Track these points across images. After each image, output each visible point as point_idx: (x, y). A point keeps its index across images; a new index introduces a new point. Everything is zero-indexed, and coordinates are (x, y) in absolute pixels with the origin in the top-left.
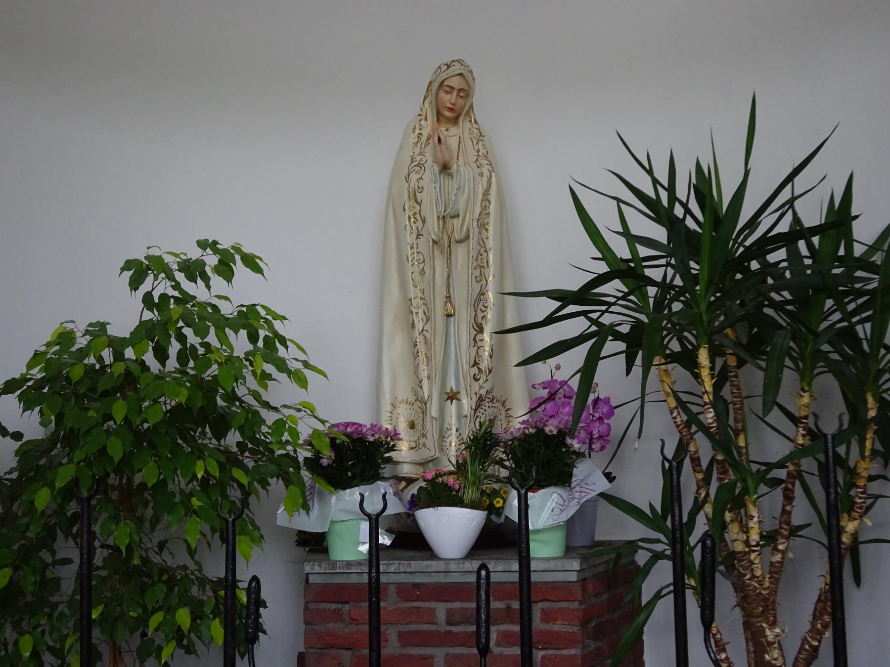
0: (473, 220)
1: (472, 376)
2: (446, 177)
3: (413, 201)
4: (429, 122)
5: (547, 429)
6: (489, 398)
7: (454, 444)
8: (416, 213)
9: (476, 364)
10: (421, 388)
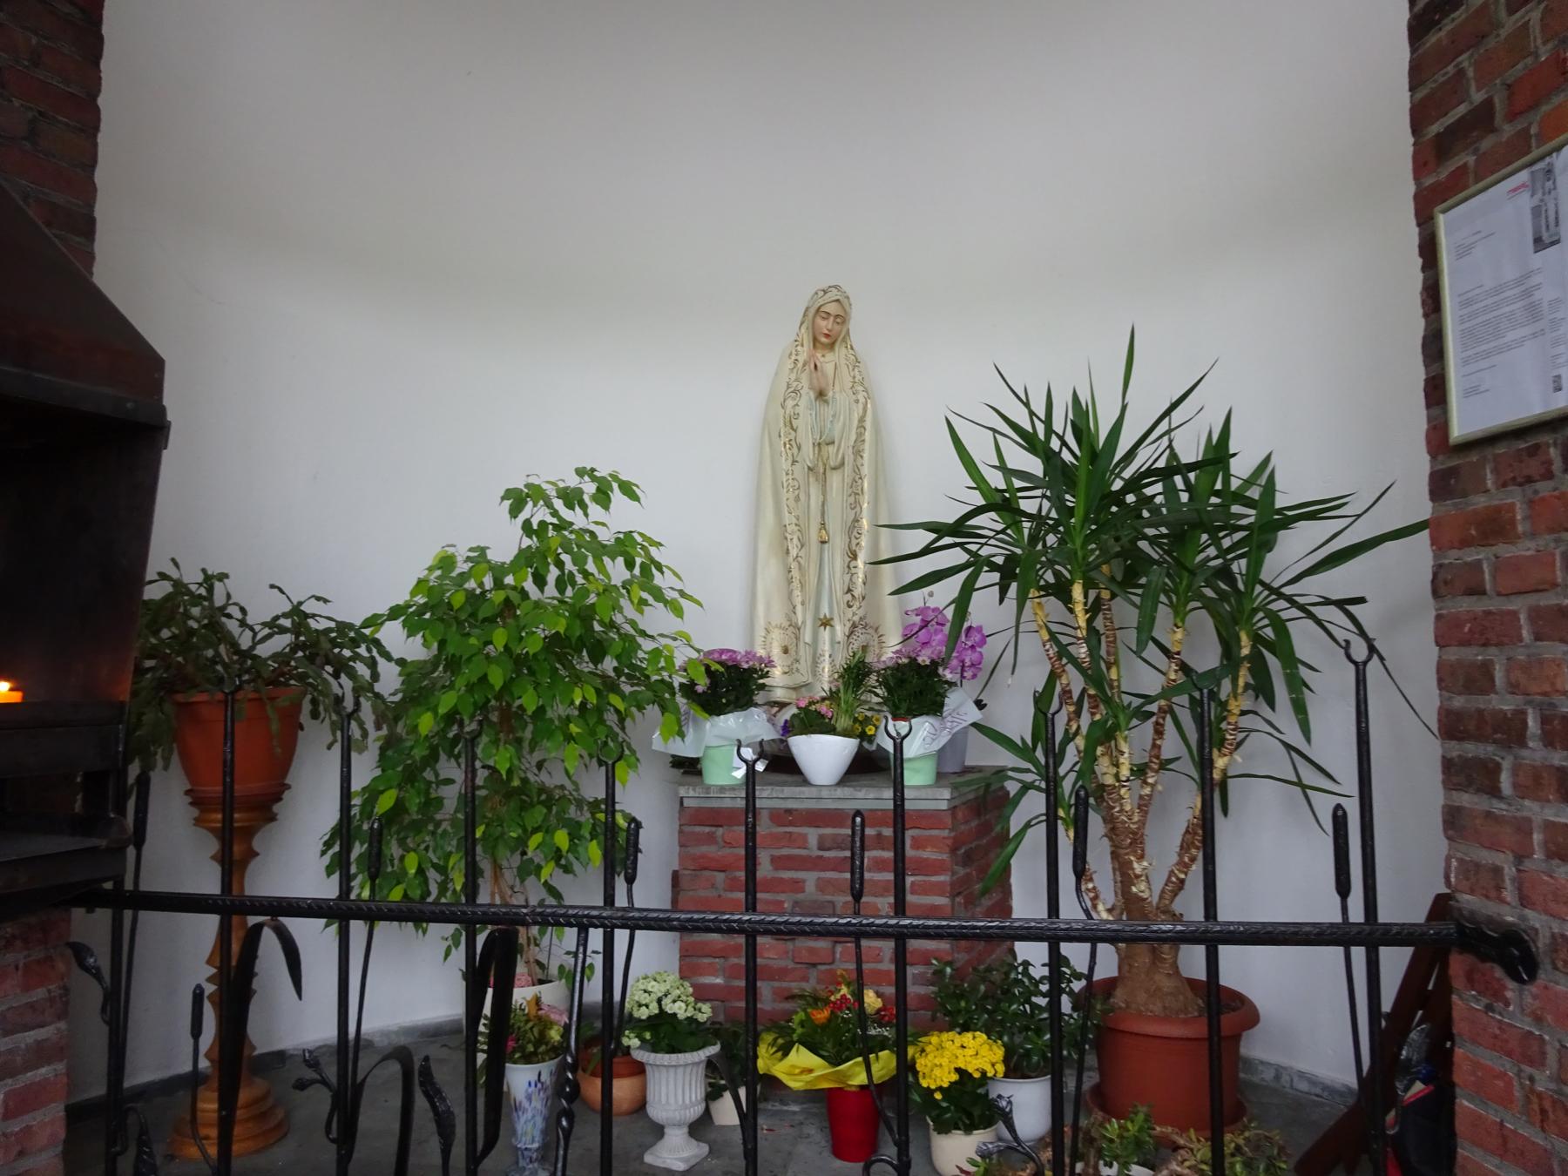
3: (788, 428)
4: (805, 348)
7: (826, 670)
9: (849, 590)
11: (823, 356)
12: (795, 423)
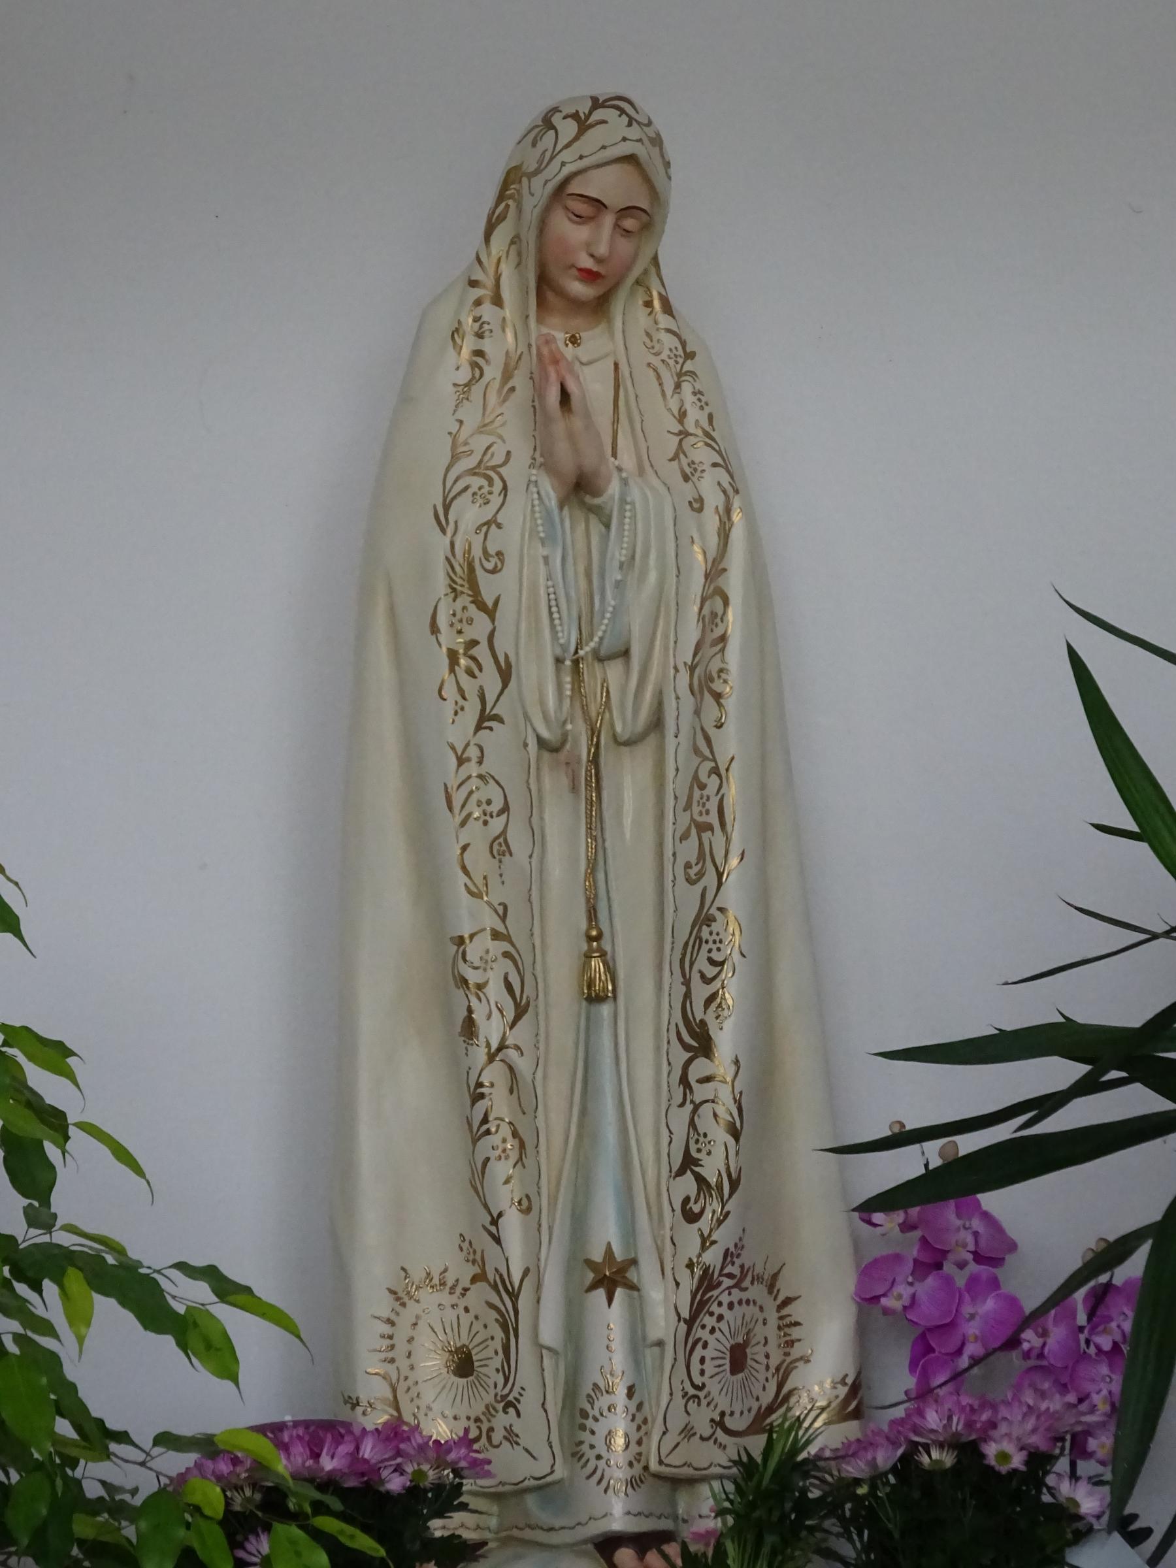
0: (676, 670)
1: (677, 1206)
2: (579, 514)
3: (464, 600)
4: (509, 311)
5: (991, 1450)
6: (730, 1276)
7: (620, 1441)
8: (474, 643)
9: (689, 1162)
10: (497, 1240)
11: (574, 340)
12: (489, 588)
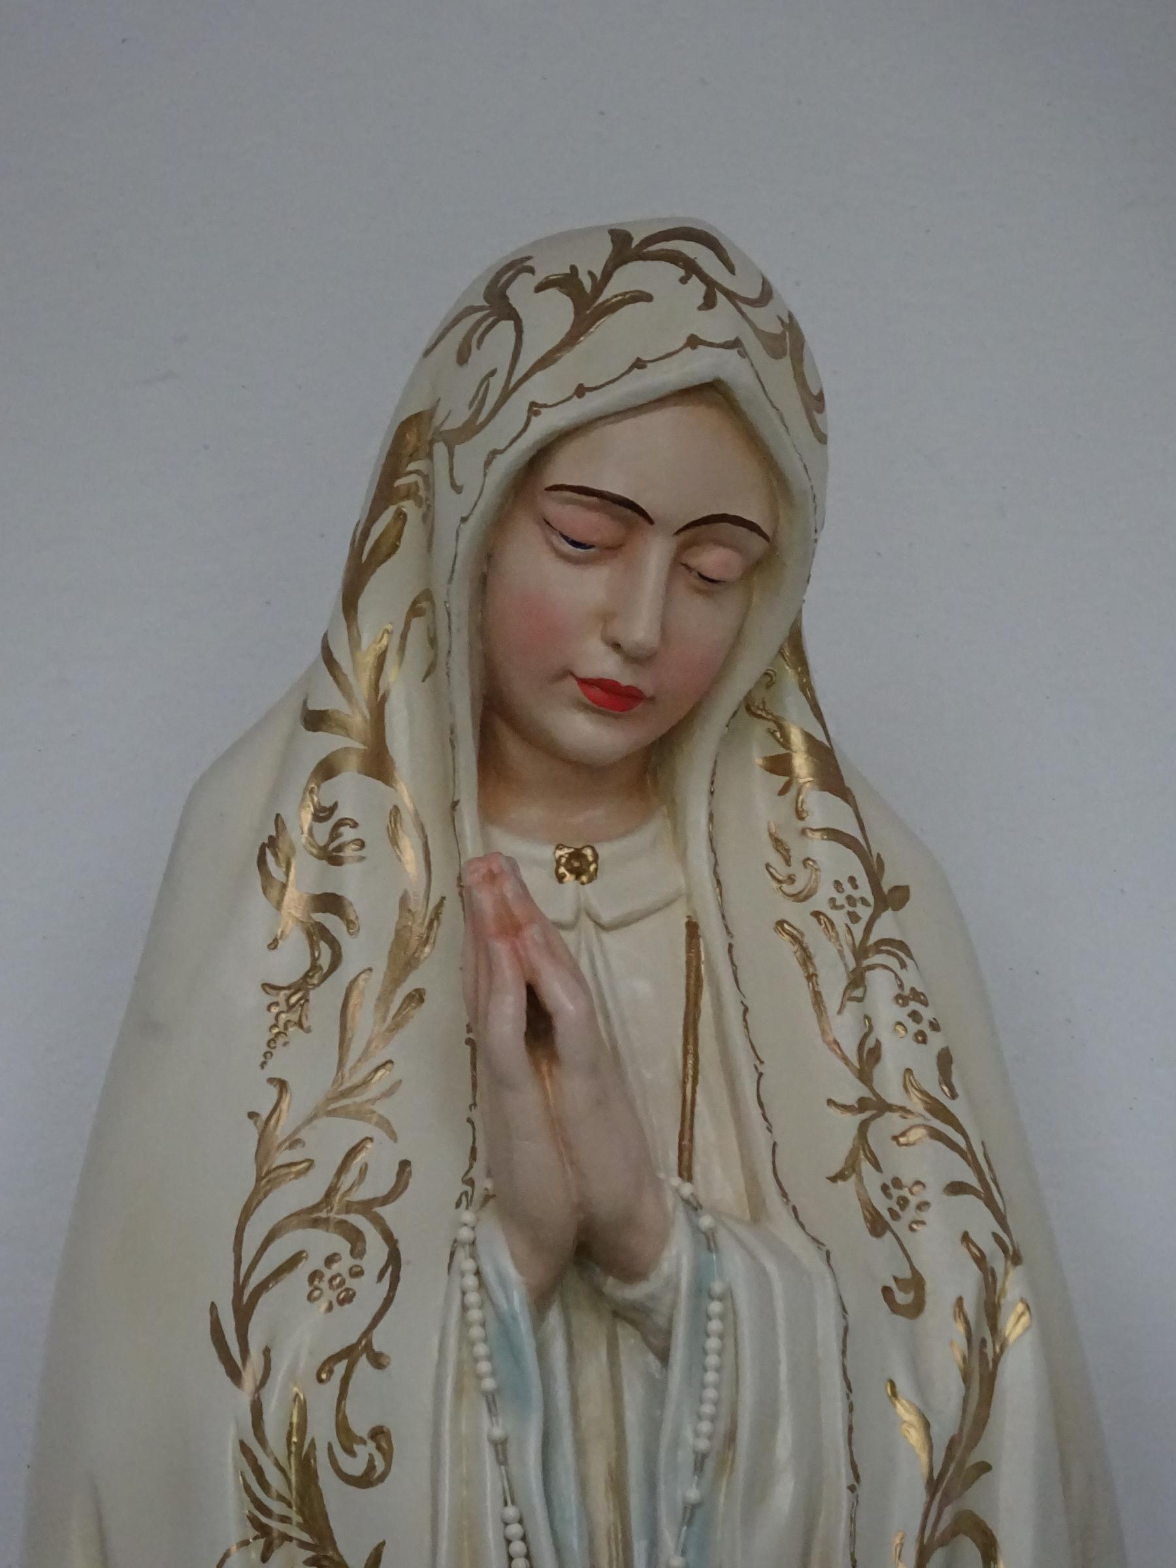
2: (592, 1327)
